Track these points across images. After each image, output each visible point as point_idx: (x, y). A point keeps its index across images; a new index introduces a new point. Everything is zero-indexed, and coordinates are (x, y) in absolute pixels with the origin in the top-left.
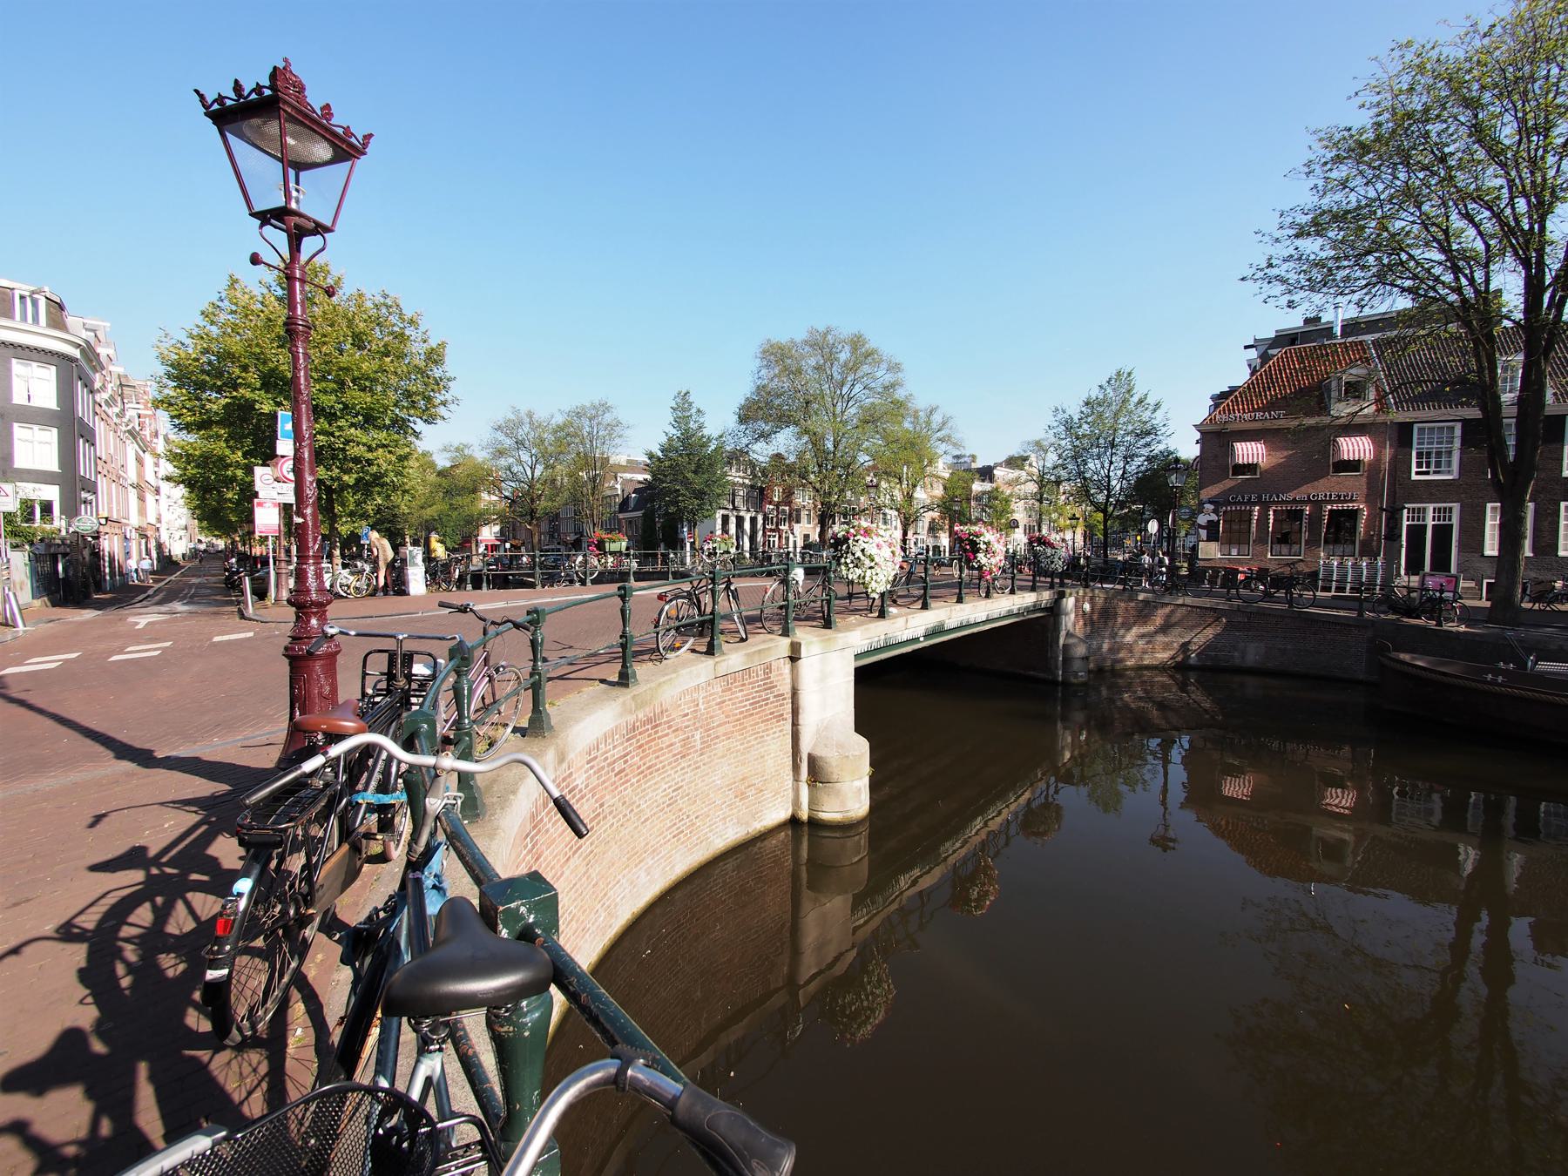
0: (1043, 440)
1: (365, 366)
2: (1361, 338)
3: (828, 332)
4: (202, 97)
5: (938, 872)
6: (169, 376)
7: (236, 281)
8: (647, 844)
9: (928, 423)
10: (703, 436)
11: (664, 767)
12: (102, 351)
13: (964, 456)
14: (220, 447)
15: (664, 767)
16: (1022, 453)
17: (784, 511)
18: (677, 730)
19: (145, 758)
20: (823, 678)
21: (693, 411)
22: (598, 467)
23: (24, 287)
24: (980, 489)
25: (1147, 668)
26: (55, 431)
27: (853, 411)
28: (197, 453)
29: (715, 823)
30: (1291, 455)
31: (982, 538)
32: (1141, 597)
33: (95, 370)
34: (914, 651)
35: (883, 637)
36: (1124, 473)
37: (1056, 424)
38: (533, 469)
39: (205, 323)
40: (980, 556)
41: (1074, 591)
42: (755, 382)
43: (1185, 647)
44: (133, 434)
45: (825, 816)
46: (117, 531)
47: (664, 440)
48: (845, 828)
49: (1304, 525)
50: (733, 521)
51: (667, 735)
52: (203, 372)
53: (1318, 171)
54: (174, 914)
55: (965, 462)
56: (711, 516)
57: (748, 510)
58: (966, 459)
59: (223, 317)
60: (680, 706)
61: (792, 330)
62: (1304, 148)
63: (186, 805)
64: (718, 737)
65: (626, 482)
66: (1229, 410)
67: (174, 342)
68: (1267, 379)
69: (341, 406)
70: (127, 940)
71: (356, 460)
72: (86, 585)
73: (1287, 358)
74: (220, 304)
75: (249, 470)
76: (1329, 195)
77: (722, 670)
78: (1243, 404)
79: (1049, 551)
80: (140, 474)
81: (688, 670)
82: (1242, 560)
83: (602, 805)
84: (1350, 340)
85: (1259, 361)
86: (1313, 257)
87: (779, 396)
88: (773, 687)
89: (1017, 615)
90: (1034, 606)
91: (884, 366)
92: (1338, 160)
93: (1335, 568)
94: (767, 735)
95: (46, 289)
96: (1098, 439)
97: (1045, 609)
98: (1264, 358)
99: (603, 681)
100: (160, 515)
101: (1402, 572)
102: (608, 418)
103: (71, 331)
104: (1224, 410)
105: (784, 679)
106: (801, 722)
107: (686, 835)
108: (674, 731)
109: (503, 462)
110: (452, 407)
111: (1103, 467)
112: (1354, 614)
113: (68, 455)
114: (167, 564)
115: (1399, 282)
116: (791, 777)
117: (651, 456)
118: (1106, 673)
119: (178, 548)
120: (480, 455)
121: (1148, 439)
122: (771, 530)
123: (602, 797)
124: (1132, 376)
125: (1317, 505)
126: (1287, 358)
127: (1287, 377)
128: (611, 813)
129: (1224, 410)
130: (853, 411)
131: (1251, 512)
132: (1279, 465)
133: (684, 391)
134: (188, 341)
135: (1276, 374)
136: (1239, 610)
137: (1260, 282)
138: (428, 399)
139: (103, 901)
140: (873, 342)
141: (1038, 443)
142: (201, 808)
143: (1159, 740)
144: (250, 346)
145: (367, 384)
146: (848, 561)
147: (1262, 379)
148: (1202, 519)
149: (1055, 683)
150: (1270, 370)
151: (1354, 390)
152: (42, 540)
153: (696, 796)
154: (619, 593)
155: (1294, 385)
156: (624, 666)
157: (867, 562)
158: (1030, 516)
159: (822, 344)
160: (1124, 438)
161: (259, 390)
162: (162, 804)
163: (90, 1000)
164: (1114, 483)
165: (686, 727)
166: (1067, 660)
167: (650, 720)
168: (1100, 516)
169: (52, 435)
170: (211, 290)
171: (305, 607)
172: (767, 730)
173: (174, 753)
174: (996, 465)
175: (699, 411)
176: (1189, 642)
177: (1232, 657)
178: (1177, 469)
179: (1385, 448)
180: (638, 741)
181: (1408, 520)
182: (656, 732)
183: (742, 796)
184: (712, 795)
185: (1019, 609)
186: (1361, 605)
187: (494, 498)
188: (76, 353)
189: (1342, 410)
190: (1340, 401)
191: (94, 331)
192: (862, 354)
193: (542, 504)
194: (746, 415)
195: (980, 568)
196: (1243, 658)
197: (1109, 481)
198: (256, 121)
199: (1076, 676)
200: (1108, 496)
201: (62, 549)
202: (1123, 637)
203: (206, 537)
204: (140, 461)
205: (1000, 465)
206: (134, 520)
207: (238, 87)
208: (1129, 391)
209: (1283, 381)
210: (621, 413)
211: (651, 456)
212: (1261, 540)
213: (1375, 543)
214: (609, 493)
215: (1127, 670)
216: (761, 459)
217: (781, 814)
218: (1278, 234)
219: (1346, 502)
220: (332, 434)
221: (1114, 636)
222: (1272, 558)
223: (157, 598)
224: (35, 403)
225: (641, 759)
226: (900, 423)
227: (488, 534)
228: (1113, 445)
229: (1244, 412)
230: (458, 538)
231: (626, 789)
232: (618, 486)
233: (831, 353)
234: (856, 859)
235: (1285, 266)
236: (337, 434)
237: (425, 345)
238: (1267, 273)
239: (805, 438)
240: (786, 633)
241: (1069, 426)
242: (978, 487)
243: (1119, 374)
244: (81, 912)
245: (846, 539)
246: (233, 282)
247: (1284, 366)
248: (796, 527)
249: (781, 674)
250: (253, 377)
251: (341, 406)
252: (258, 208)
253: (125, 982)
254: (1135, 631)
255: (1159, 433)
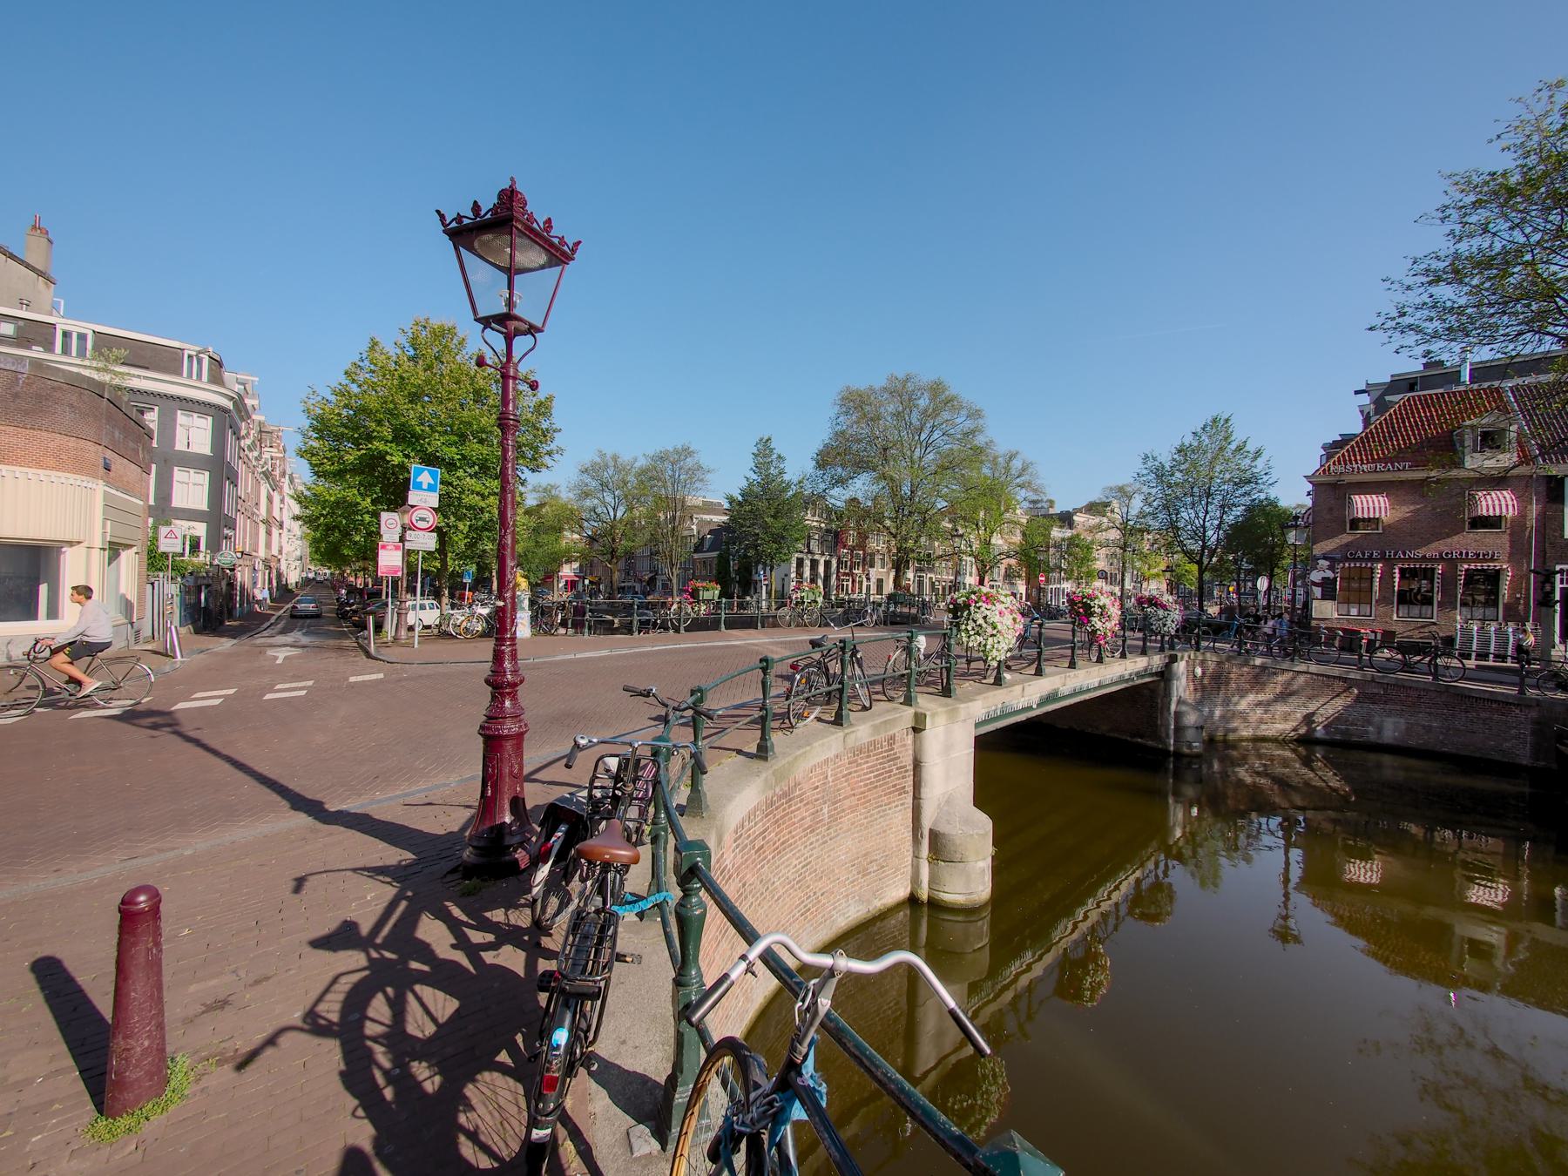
0: (1127, 485)
1: (484, 421)
2: (1496, 384)
3: (907, 380)
4: (442, 217)
5: (1049, 958)
6: (315, 429)
7: (376, 344)
8: (779, 923)
9: (1007, 469)
10: (782, 482)
11: (795, 842)
12: (249, 402)
13: (1042, 501)
14: (352, 494)
15: (795, 842)
16: (1105, 500)
17: (857, 554)
18: (808, 803)
19: (314, 809)
20: (948, 748)
21: (774, 456)
22: (678, 508)
23: (192, 347)
24: (1061, 535)
25: (1264, 739)
26: (207, 474)
27: (931, 456)
28: (332, 499)
29: (839, 900)
30: (1418, 510)
31: (1096, 602)
32: (1258, 661)
33: (243, 420)
34: (1028, 720)
35: (1000, 706)
36: (1221, 523)
37: (1145, 472)
38: (615, 509)
39: (347, 382)
40: (1095, 620)
41: (1186, 654)
42: (833, 428)
43: (1308, 719)
44: (267, 475)
45: (948, 897)
46: (248, 563)
47: (744, 484)
48: (969, 911)
49: (1436, 585)
50: (807, 563)
51: (799, 809)
52: (343, 425)
53: (1455, 215)
54: (409, 1009)
55: (1042, 507)
56: (788, 560)
57: (823, 554)
58: (1043, 504)
59: (361, 378)
60: (811, 778)
61: (871, 377)
62: (1438, 193)
63: (378, 874)
64: (843, 811)
65: (702, 523)
66: (1345, 461)
67: (319, 398)
68: (1387, 428)
69: (459, 457)
70: (375, 1039)
71: (470, 508)
72: (221, 613)
73: (1411, 405)
74: (361, 364)
75: (376, 515)
76: (1465, 240)
77: (851, 741)
78: (1361, 455)
79: (1161, 613)
80: (270, 510)
81: (821, 742)
82: (1366, 619)
83: (744, 885)
84: (1486, 385)
85: (1372, 406)
86: (1449, 304)
87: (859, 441)
88: (896, 759)
89: (1127, 681)
90: (1146, 670)
91: (964, 412)
92: (1477, 204)
93: (1475, 634)
94: (890, 809)
95: (211, 349)
96: (1192, 488)
97: (1156, 674)
98: (1380, 405)
99: (739, 752)
100: (281, 547)
101: (1557, 639)
102: (690, 462)
103: (227, 386)
104: (1339, 461)
105: (907, 750)
106: (923, 796)
107: (812, 913)
108: (805, 805)
109: (588, 503)
110: (556, 457)
111: (1198, 517)
112: (1512, 691)
113: (216, 495)
114: (283, 592)
115: (1551, 329)
116: (911, 853)
117: (731, 500)
118: (1219, 745)
119: (293, 577)
120: (566, 495)
121: (1247, 488)
122: (845, 574)
123: (743, 877)
124: (1230, 423)
125: (1451, 562)
126: (1411, 405)
127: (1411, 426)
128: (751, 892)
129: (1339, 461)
130: (931, 456)
131: (1372, 570)
132: (1405, 519)
133: (766, 438)
134: (333, 398)
135: (1398, 423)
136: (1373, 680)
137: (1389, 333)
138: (536, 449)
139: (337, 987)
140: (954, 387)
141: (1121, 489)
142: (394, 879)
143: (1280, 819)
144: (385, 402)
145: (484, 436)
146: (969, 628)
147: (1382, 428)
148: (1316, 576)
149: (1166, 753)
150: (1391, 419)
151: (1490, 440)
152: (191, 574)
153: (822, 872)
154: (761, 665)
155: (1420, 434)
156: (763, 738)
157: (989, 630)
158: (1111, 564)
159: (901, 391)
160: (1223, 487)
161: (391, 442)
162: (354, 870)
163: (360, 1112)
164: (1210, 533)
165: (817, 800)
166: (1179, 729)
167: (785, 795)
168: (1194, 568)
169: (204, 478)
170: (351, 351)
171: (502, 688)
172: (889, 803)
173: (344, 807)
174: (1077, 511)
175: (779, 457)
176: (1313, 714)
177: (1367, 732)
178: (1296, 527)
179: (1531, 504)
180: (775, 816)
181: (1562, 583)
182: (790, 806)
183: (864, 873)
184: (837, 871)
185: (1131, 674)
186: (1522, 679)
187: (576, 536)
188: (229, 405)
189: (1477, 462)
190: (1475, 451)
191: (244, 384)
192: (942, 400)
193: (624, 544)
194: (824, 460)
195: (1094, 632)
196: (1379, 733)
197: (1205, 532)
198: (488, 237)
199: (1190, 746)
200: (1204, 547)
201: (205, 582)
202: (1236, 704)
203: (315, 566)
204: (270, 499)
205: (1080, 510)
206: (262, 553)
207: (476, 207)
208: (1226, 439)
209: (1406, 430)
210: (704, 459)
211: (731, 500)
212: (1385, 600)
213: (1521, 607)
214: (686, 533)
215: (1242, 740)
216: (839, 504)
217: (900, 892)
218: (1409, 281)
219: (1487, 561)
220: (450, 484)
221: (1227, 702)
222: (1398, 620)
223: (280, 626)
224: (195, 449)
225: (776, 835)
226: (979, 469)
227: (568, 571)
228: (1209, 495)
229: (1362, 463)
230: (541, 575)
231: (763, 867)
232: (694, 527)
233: (910, 400)
234: (979, 946)
235: (1418, 314)
236: (455, 483)
237: (535, 399)
238: (1398, 323)
239: (883, 483)
240: (908, 701)
241: (1160, 474)
242: (1057, 533)
243: (1214, 421)
244: (320, 999)
245: (967, 606)
246: (374, 345)
247: (1407, 414)
248: (872, 571)
249: (905, 745)
250: (387, 432)
251: (459, 457)
252: (481, 314)
253: (388, 1093)
254: (1251, 697)
255: (1260, 481)
